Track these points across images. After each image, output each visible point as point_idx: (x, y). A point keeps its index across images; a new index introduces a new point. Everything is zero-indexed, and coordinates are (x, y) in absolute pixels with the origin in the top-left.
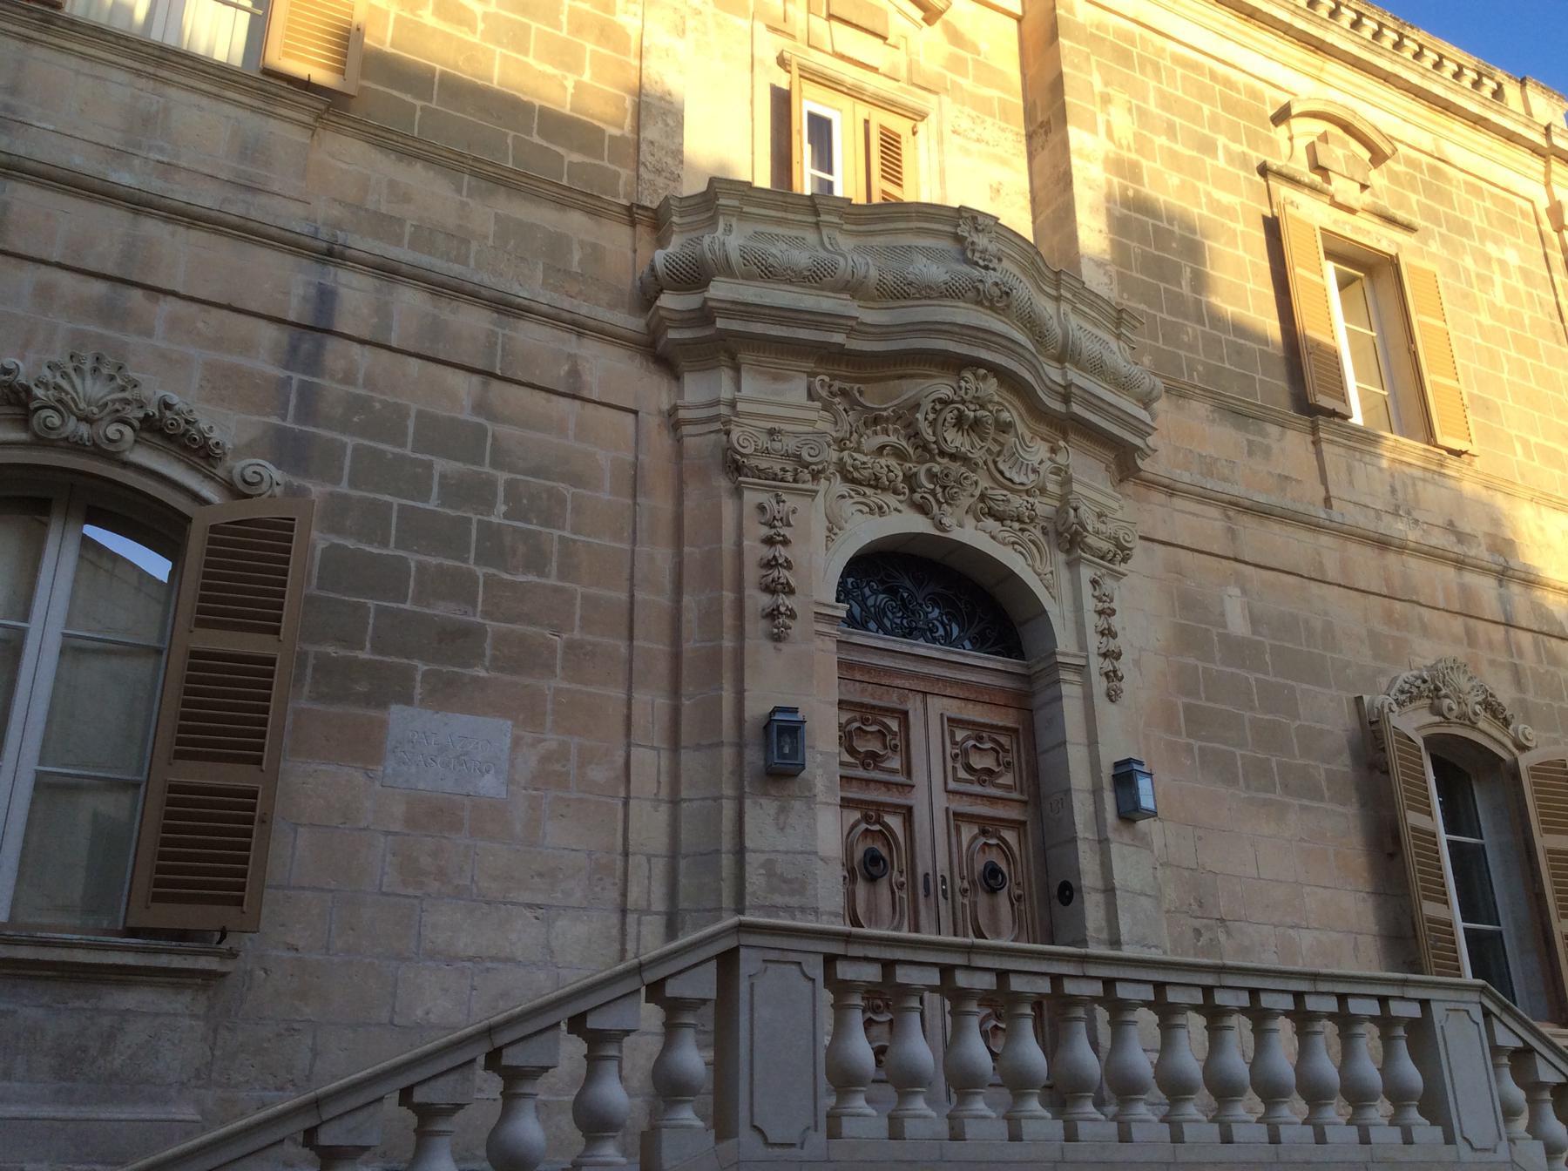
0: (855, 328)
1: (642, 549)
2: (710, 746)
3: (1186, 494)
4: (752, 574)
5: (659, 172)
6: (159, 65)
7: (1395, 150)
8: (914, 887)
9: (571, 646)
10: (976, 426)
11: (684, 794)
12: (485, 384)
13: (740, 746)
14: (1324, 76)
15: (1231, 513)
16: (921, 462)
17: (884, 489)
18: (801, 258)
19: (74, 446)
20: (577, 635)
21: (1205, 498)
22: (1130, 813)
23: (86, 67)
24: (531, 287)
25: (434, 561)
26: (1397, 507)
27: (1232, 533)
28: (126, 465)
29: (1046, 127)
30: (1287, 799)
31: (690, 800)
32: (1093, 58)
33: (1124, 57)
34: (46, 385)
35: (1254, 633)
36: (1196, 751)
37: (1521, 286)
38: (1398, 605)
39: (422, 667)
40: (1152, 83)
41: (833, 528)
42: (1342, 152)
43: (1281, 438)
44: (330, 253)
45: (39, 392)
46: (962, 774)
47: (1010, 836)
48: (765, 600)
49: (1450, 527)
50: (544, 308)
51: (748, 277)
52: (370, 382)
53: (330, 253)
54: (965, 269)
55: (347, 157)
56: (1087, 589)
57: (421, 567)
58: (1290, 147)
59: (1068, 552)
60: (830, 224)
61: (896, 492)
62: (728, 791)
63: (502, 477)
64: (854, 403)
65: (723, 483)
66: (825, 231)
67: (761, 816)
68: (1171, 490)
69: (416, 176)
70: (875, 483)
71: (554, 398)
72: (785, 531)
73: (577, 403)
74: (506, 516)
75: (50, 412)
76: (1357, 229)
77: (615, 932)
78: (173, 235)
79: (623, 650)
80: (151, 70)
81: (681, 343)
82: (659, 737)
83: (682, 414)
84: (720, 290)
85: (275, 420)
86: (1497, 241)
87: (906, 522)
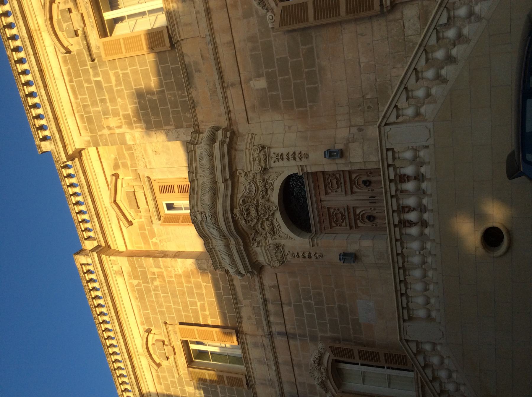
0: (238, 245)
3: (227, 106)
10: (248, 210)
14: (37, 28)
15: (226, 85)
17: (273, 225)
18: (226, 258)
21: (225, 98)
22: (341, 154)
25: (327, 315)
27: (233, 85)
28: (327, 366)
32: (99, 133)
35: (263, 76)
36: (312, 104)
51: (236, 266)
55: (247, 327)
56: (277, 164)
63: (303, 301)
67: (356, 128)
68: (229, 112)
70: (272, 229)
74: (312, 300)
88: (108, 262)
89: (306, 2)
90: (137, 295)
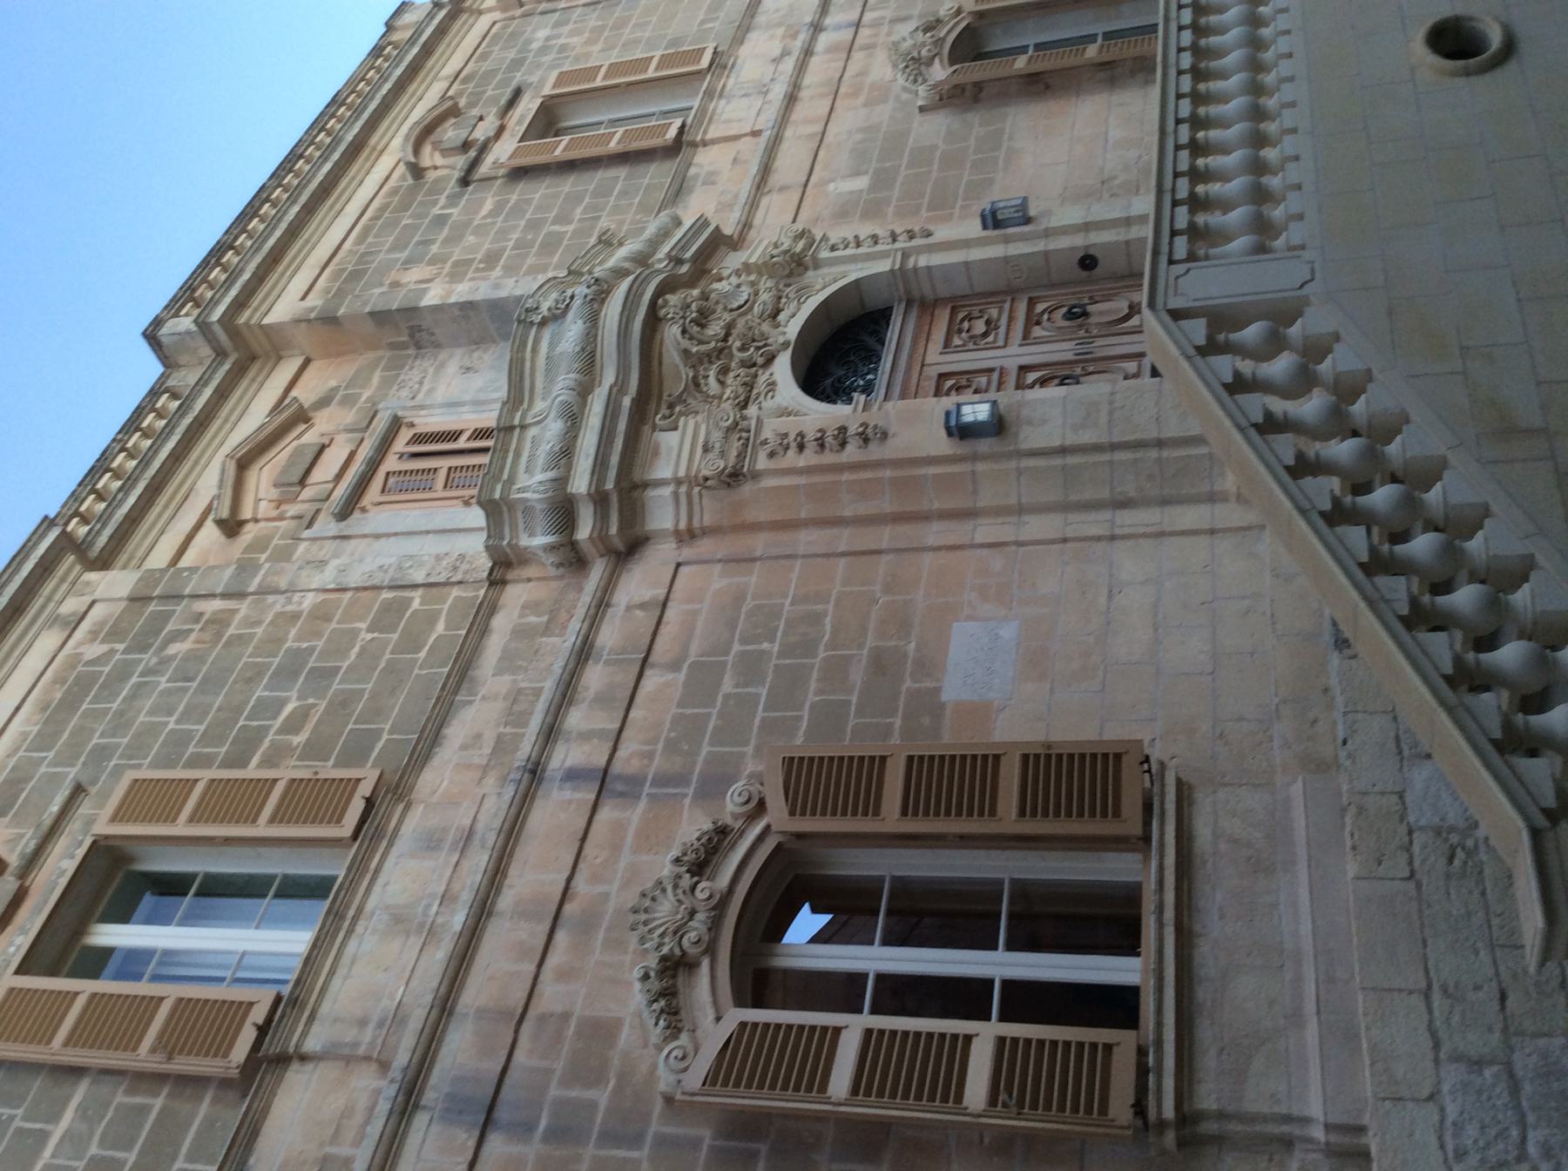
0: (619, 388)
1: (801, 550)
2: (974, 482)
4: (829, 458)
5: (455, 568)
6: (343, 918)
7: (451, 98)
8: (1086, 361)
9: (888, 589)
11: (1013, 501)
12: (653, 666)
13: (975, 458)
14: (379, 148)
16: (731, 356)
18: (555, 427)
19: (715, 925)
20: (878, 588)
23: (341, 972)
24: (564, 643)
26: (760, 92)
29: (414, 331)
30: (1004, 148)
31: (1020, 496)
33: (356, 275)
34: (660, 945)
37: (570, 27)
38: (842, 90)
39: (908, 684)
40: (381, 256)
41: (785, 412)
42: (451, 133)
43: (701, 166)
44: (533, 772)
45: (665, 950)
46: (991, 338)
47: (1040, 307)
48: (851, 448)
49: (776, 61)
50: (586, 625)
52: (653, 741)
53: (533, 772)
54: (570, 316)
57: (819, 692)
58: (442, 166)
59: (806, 269)
60: (523, 417)
61: (756, 376)
62: (1013, 464)
64: (680, 399)
65: (747, 489)
66: (529, 420)
67: (1032, 438)
69: (457, 732)
70: (749, 386)
71: (665, 619)
72: (792, 437)
73: (670, 604)
75: (685, 941)
76: (519, 122)
77: (1130, 543)
78: (511, 887)
79: (890, 557)
80: (347, 923)
81: (620, 529)
82: (968, 526)
83: (682, 525)
84: (580, 484)
85: (687, 801)
86: (529, 41)
87: (782, 369)
88: (62, 580)
89: (883, 759)
90: (59, 695)
